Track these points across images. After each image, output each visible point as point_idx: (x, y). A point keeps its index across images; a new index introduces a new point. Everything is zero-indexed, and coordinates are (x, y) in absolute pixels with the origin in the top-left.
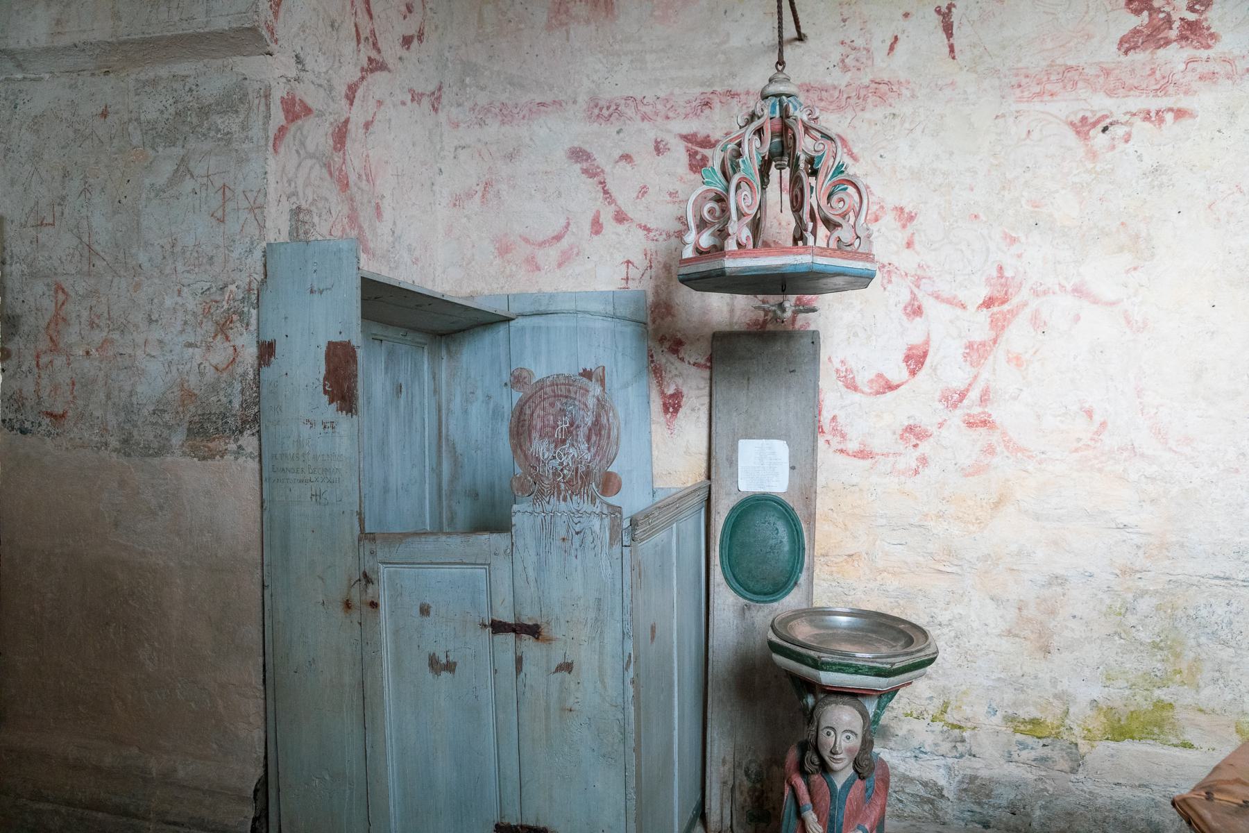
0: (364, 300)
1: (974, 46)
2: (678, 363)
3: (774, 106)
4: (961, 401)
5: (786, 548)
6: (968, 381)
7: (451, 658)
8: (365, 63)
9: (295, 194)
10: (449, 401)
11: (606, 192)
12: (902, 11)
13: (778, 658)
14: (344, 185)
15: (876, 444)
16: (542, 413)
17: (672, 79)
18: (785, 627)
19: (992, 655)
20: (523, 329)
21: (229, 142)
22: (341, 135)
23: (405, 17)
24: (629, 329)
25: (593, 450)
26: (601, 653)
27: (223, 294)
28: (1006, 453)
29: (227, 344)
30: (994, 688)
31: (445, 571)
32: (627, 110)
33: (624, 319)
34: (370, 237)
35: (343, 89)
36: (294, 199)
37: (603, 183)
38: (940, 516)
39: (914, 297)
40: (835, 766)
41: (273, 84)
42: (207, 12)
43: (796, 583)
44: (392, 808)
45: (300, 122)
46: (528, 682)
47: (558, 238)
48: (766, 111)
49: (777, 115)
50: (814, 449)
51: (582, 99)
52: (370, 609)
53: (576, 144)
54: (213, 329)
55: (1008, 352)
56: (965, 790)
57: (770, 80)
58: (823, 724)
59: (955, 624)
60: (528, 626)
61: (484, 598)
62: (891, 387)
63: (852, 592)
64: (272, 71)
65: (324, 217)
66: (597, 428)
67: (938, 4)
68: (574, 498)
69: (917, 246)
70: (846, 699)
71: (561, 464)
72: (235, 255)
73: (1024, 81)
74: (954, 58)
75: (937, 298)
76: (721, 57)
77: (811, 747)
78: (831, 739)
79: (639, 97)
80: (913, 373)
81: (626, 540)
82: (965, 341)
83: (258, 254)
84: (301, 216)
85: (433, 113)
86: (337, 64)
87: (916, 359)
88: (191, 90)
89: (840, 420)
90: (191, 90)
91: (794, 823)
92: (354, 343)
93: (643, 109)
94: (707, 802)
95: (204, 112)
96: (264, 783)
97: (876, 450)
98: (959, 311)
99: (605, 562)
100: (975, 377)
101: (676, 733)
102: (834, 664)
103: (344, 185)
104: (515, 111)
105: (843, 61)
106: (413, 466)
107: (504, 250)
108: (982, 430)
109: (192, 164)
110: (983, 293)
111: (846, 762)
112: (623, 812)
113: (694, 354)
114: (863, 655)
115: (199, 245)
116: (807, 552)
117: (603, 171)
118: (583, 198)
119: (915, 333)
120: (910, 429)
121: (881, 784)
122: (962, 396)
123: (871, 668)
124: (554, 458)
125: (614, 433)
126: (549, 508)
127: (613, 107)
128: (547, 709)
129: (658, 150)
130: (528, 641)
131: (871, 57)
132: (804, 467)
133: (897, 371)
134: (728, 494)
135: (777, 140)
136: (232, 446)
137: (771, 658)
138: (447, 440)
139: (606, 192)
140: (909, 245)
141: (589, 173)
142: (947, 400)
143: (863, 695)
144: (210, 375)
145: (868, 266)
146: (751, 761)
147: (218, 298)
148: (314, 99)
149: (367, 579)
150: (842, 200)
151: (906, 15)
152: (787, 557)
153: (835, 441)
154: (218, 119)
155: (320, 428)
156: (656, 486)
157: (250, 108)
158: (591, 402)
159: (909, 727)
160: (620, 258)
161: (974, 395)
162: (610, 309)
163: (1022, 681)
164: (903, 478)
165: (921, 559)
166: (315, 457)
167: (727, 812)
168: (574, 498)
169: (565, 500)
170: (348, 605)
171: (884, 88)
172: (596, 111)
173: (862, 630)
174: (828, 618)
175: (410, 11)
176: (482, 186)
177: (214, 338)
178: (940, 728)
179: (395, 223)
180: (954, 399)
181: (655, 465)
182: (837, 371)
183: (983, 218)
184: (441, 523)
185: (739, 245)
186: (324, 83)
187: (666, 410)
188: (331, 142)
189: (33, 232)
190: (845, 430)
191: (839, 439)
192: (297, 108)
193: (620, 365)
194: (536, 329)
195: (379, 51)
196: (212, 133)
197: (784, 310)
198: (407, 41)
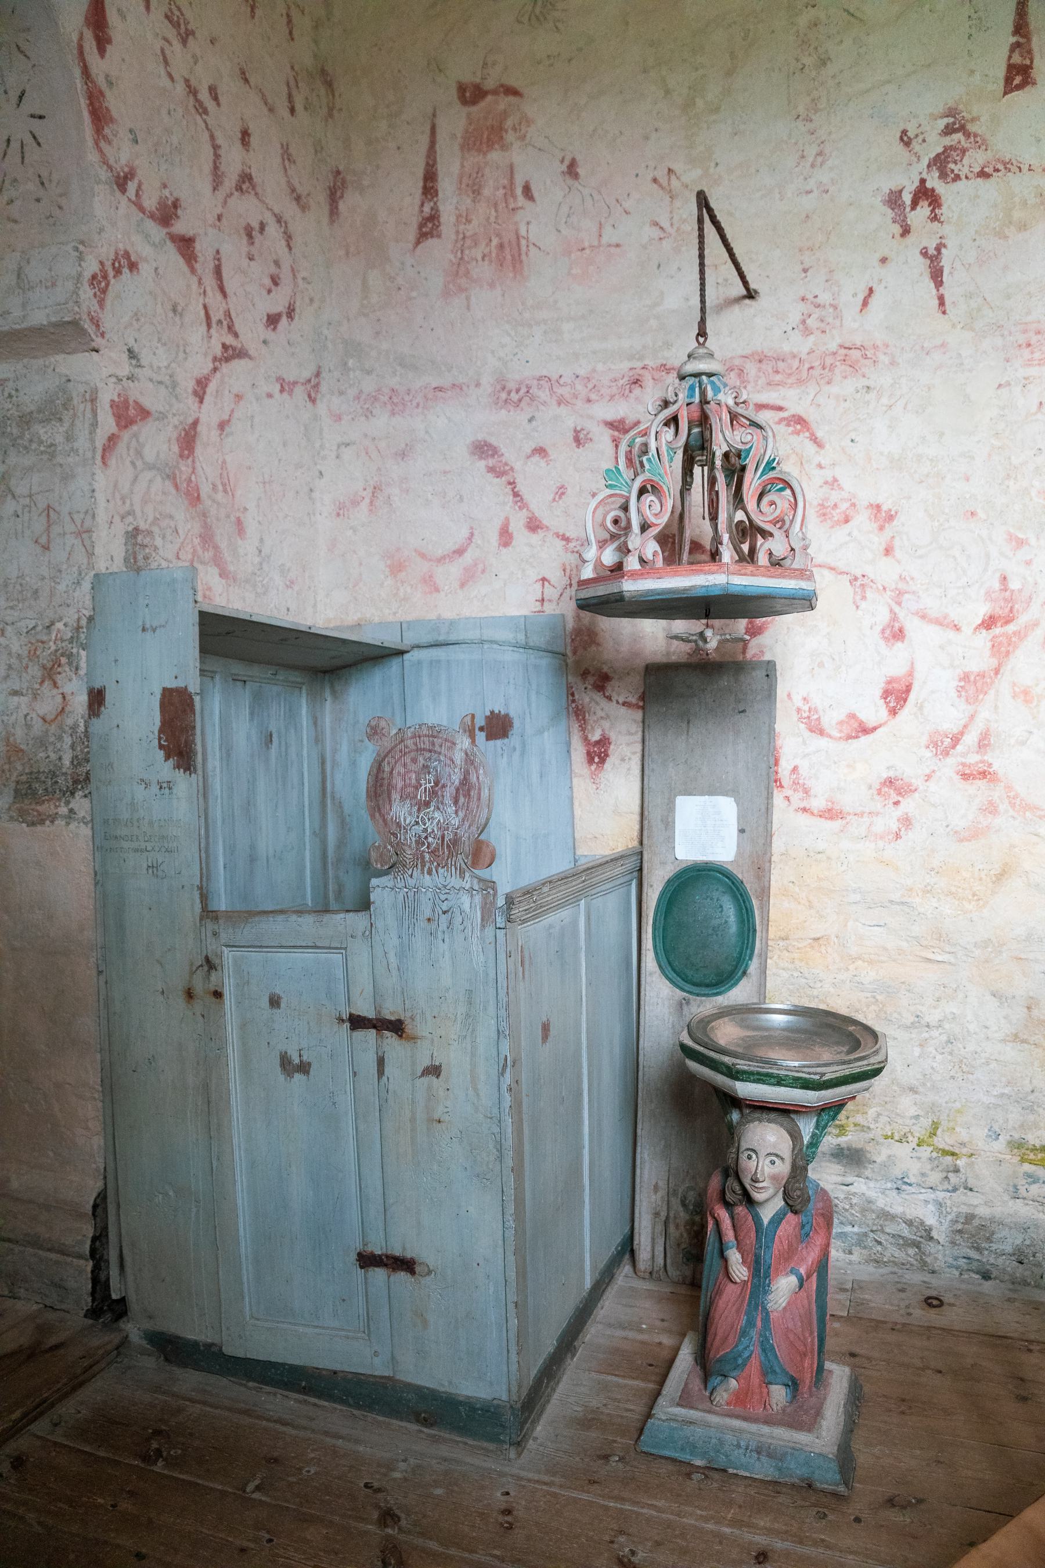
0: (203, 635)
1: (969, 296)
2: (604, 703)
3: (692, 388)
4: (954, 747)
5: (733, 928)
6: (963, 722)
7: (305, 1058)
8: (218, 351)
9: (131, 513)
10: (335, 751)
11: (516, 495)
12: (878, 256)
13: (693, 1065)
14: (194, 498)
15: (847, 802)
16: (402, 770)
17: (594, 352)
18: (705, 1029)
19: (993, 1065)
20: (419, 662)
21: (52, 456)
22: (188, 440)
23: (269, 291)
24: (545, 662)
25: (461, 814)
26: (473, 1055)
27: (50, 633)
28: (1011, 813)
29: (55, 691)
30: (996, 1106)
31: (297, 955)
32: (540, 393)
33: (539, 649)
34: (229, 559)
35: (191, 385)
36: (130, 519)
37: (512, 483)
38: (928, 891)
39: (894, 618)
40: (758, 1196)
41: (100, 385)
42: (24, 305)
43: (744, 973)
44: (241, 1230)
45: (135, 428)
46: (391, 1087)
47: (460, 552)
48: (681, 396)
49: (697, 400)
50: (768, 810)
51: (487, 380)
52: (214, 999)
53: (480, 437)
54: (39, 674)
55: (1014, 684)
56: (960, 1231)
57: (689, 356)
58: (744, 1145)
59: (947, 1026)
60: (390, 1022)
61: (342, 987)
62: (865, 730)
63: (819, 985)
64: (99, 372)
65: (169, 538)
66: (465, 787)
67: (924, 244)
68: (441, 871)
69: (898, 553)
70: (773, 1115)
71: (425, 830)
72: (62, 587)
73: (1034, 339)
74: (944, 313)
75: (923, 617)
76: (653, 323)
77: (732, 1172)
78: (752, 1164)
79: (555, 377)
80: (893, 712)
81: (500, 921)
82: (959, 671)
83: (86, 586)
84: (140, 538)
85: (309, 404)
86: (181, 355)
87: (897, 695)
88: (10, 396)
89: (803, 771)
90: (10, 396)
91: (717, 1262)
92: (192, 689)
93: (560, 391)
94: (636, 1237)
95: (26, 420)
96: (102, 1198)
97: (847, 809)
98: (951, 634)
99: (475, 947)
100: (972, 717)
101: (586, 1152)
102: (752, 1073)
103: (194, 498)
104: (407, 398)
105: (804, 322)
106: (289, 829)
107: (397, 568)
108: (981, 783)
109: (13, 482)
110: (983, 610)
111: (771, 1191)
112: (501, 1242)
113: (624, 691)
114: (791, 1062)
115: (22, 577)
116: (758, 934)
117: (512, 469)
118: (490, 503)
119: (894, 662)
120: (890, 782)
121: (820, 1220)
122: (956, 740)
123: (797, 1079)
124: (417, 823)
125: (485, 793)
126: (411, 882)
127: (523, 390)
128: (413, 1120)
129: (578, 441)
130: (390, 1039)
131: (839, 316)
132: (756, 829)
133: (873, 711)
134: (663, 863)
135: (696, 430)
136: (63, 810)
137: (684, 1064)
138: (333, 798)
139: (516, 495)
140: (888, 551)
141: (496, 471)
142: (936, 745)
143: (796, 1112)
144: (38, 727)
145: (804, 585)
146: (690, 1188)
147: (45, 638)
148: (151, 397)
149: (210, 965)
150: (772, 503)
151: (884, 260)
152: (734, 940)
153: (796, 798)
154: (41, 430)
155: (155, 788)
156: (578, 853)
157: (75, 415)
158: (459, 757)
159: (889, 1152)
160: (533, 575)
161: (970, 739)
162: (521, 637)
163: (1031, 1097)
164: (881, 844)
165: (904, 944)
166: (151, 823)
167: (660, 1249)
168: (441, 871)
169: (430, 873)
170: (190, 995)
171: (855, 354)
172: (504, 395)
173: (805, 1031)
174: (751, 1016)
175: (276, 284)
176: (370, 490)
177: (42, 682)
178: (927, 1154)
179: (261, 540)
180: (945, 744)
181: (578, 827)
182: (799, 710)
183: (981, 514)
184: (326, 896)
185: (642, 561)
186: (166, 379)
187: (590, 760)
188: (176, 449)
189: (832, 189)
190: (809, 783)
191: (801, 794)
192: (132, 412)
193: (533, 705)
194: (434, 663)
195: (236, 335)
196: (34, 446)
197: (705, 641)
198: (273, 320)
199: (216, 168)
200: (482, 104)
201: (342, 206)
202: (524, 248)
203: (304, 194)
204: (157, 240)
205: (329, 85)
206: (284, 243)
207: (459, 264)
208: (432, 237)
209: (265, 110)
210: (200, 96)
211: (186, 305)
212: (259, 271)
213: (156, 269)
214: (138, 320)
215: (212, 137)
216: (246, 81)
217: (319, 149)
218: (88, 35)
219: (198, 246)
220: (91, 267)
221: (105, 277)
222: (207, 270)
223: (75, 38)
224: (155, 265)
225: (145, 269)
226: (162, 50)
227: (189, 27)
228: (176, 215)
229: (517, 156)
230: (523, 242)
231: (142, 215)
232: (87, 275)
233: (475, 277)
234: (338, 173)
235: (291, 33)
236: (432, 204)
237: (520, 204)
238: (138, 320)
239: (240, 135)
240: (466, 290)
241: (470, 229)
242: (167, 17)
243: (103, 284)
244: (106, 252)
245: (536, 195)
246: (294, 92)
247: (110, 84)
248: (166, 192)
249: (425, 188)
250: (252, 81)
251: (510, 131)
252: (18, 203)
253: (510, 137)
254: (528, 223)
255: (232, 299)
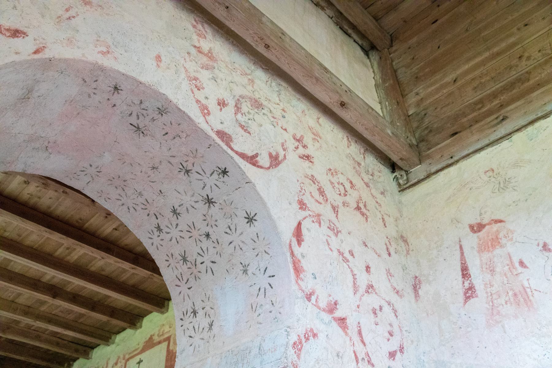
23: (388, 340)
175: (392, 335)
198: (392, 355)
199: (355, 284)
200: (484, 230)
201: (420, 292)
202: (530, 293)
203: (400, 290)
204: (327, 322)
205: (405, 241)
206: (393, 314)
207: (492, 309)
208: (473, 297)
209: (376, 256)
210: (345, 255)
211: (344, 352)
212: (383, 330)
213: (327, 335)
214: (318, 363)
215: (352, 271)
216: (366, 246)
217: (405, 268)
218: (294, 240)
219: (348, 321)
220: (294, 338)
221: (301, 343)
222: (354, 333)
223: (288, 242)
224: (326, 334)
225: (321, 336)
226: (327, 241)
227: (339, 230)
228: (336, 308)
229: (510, 248)
230: (528, 290)
231: (319, 310)
232: (291, 342)
233: (504, 313)
234: (416, 277)
235: (385, 224)
236: (469, 281)
237: (520, 271)
238: (318, 363)
239: (365, 269)
240: (501, 322)
241: (494, 290)
242: (328, 227)
243: (300, 346)
244: (301, 331)
245: (528, 265)
246: (389, 247)
247: (303, 257)
248: (331, 298)
249: (463, 274)
250: (369, 245)
251: (503, 239)
252: (262, 315)
253: (504, 241)
254: (528, 280)
255: (368, 346)
